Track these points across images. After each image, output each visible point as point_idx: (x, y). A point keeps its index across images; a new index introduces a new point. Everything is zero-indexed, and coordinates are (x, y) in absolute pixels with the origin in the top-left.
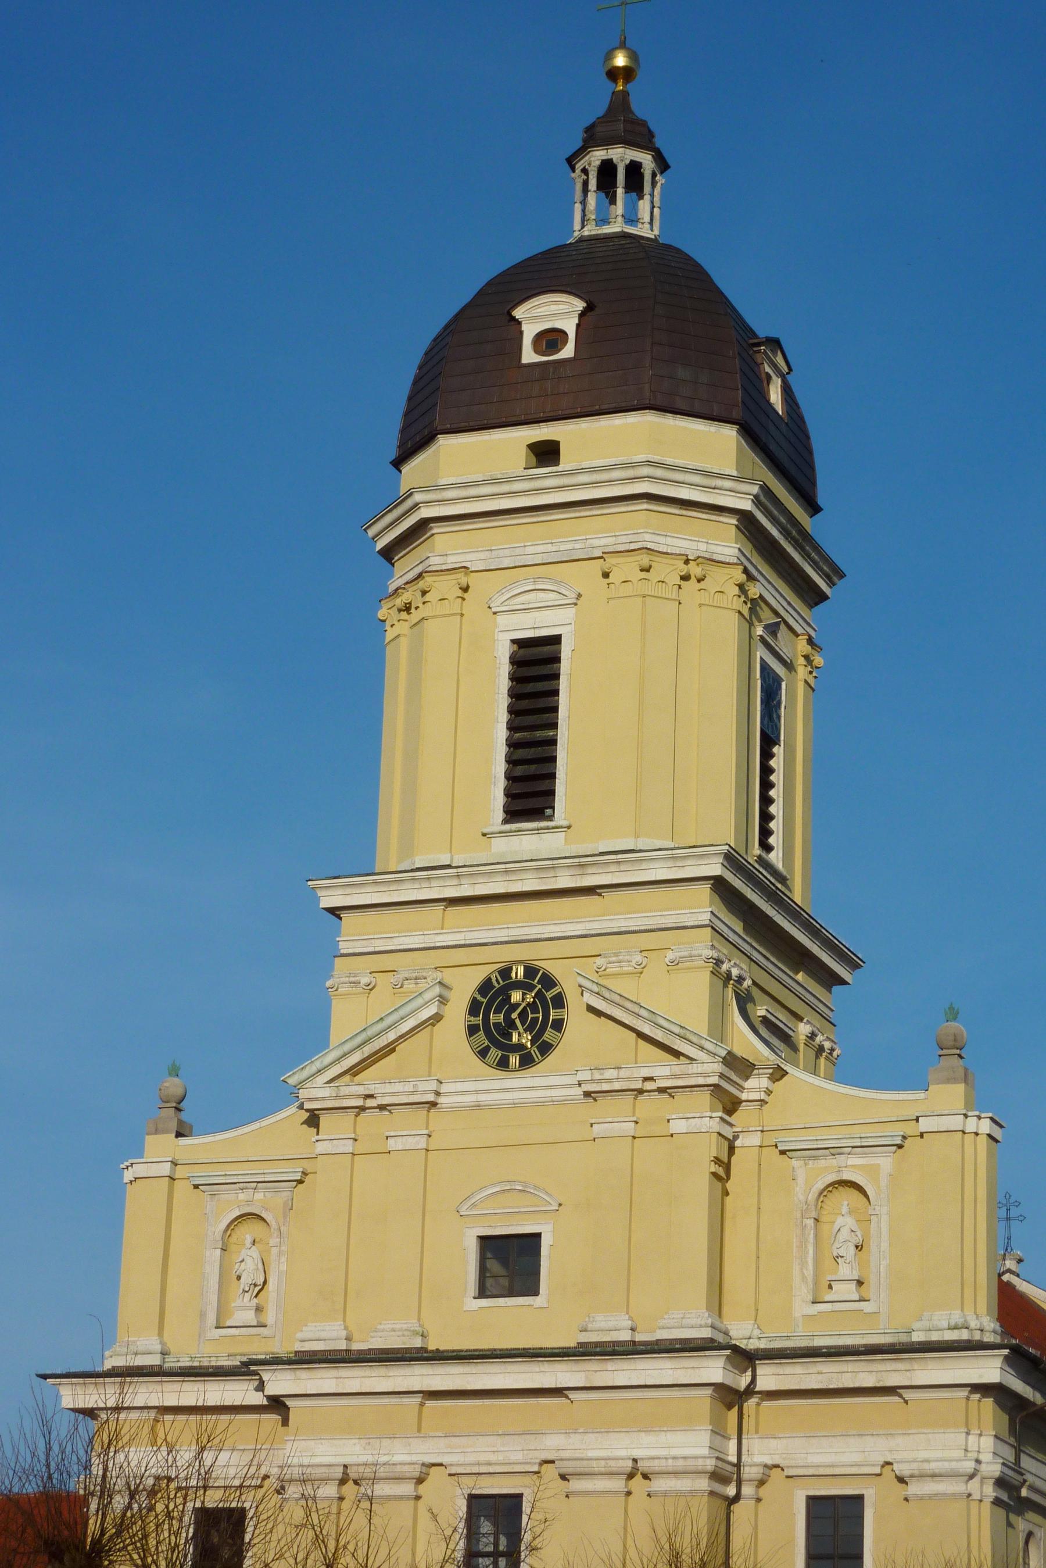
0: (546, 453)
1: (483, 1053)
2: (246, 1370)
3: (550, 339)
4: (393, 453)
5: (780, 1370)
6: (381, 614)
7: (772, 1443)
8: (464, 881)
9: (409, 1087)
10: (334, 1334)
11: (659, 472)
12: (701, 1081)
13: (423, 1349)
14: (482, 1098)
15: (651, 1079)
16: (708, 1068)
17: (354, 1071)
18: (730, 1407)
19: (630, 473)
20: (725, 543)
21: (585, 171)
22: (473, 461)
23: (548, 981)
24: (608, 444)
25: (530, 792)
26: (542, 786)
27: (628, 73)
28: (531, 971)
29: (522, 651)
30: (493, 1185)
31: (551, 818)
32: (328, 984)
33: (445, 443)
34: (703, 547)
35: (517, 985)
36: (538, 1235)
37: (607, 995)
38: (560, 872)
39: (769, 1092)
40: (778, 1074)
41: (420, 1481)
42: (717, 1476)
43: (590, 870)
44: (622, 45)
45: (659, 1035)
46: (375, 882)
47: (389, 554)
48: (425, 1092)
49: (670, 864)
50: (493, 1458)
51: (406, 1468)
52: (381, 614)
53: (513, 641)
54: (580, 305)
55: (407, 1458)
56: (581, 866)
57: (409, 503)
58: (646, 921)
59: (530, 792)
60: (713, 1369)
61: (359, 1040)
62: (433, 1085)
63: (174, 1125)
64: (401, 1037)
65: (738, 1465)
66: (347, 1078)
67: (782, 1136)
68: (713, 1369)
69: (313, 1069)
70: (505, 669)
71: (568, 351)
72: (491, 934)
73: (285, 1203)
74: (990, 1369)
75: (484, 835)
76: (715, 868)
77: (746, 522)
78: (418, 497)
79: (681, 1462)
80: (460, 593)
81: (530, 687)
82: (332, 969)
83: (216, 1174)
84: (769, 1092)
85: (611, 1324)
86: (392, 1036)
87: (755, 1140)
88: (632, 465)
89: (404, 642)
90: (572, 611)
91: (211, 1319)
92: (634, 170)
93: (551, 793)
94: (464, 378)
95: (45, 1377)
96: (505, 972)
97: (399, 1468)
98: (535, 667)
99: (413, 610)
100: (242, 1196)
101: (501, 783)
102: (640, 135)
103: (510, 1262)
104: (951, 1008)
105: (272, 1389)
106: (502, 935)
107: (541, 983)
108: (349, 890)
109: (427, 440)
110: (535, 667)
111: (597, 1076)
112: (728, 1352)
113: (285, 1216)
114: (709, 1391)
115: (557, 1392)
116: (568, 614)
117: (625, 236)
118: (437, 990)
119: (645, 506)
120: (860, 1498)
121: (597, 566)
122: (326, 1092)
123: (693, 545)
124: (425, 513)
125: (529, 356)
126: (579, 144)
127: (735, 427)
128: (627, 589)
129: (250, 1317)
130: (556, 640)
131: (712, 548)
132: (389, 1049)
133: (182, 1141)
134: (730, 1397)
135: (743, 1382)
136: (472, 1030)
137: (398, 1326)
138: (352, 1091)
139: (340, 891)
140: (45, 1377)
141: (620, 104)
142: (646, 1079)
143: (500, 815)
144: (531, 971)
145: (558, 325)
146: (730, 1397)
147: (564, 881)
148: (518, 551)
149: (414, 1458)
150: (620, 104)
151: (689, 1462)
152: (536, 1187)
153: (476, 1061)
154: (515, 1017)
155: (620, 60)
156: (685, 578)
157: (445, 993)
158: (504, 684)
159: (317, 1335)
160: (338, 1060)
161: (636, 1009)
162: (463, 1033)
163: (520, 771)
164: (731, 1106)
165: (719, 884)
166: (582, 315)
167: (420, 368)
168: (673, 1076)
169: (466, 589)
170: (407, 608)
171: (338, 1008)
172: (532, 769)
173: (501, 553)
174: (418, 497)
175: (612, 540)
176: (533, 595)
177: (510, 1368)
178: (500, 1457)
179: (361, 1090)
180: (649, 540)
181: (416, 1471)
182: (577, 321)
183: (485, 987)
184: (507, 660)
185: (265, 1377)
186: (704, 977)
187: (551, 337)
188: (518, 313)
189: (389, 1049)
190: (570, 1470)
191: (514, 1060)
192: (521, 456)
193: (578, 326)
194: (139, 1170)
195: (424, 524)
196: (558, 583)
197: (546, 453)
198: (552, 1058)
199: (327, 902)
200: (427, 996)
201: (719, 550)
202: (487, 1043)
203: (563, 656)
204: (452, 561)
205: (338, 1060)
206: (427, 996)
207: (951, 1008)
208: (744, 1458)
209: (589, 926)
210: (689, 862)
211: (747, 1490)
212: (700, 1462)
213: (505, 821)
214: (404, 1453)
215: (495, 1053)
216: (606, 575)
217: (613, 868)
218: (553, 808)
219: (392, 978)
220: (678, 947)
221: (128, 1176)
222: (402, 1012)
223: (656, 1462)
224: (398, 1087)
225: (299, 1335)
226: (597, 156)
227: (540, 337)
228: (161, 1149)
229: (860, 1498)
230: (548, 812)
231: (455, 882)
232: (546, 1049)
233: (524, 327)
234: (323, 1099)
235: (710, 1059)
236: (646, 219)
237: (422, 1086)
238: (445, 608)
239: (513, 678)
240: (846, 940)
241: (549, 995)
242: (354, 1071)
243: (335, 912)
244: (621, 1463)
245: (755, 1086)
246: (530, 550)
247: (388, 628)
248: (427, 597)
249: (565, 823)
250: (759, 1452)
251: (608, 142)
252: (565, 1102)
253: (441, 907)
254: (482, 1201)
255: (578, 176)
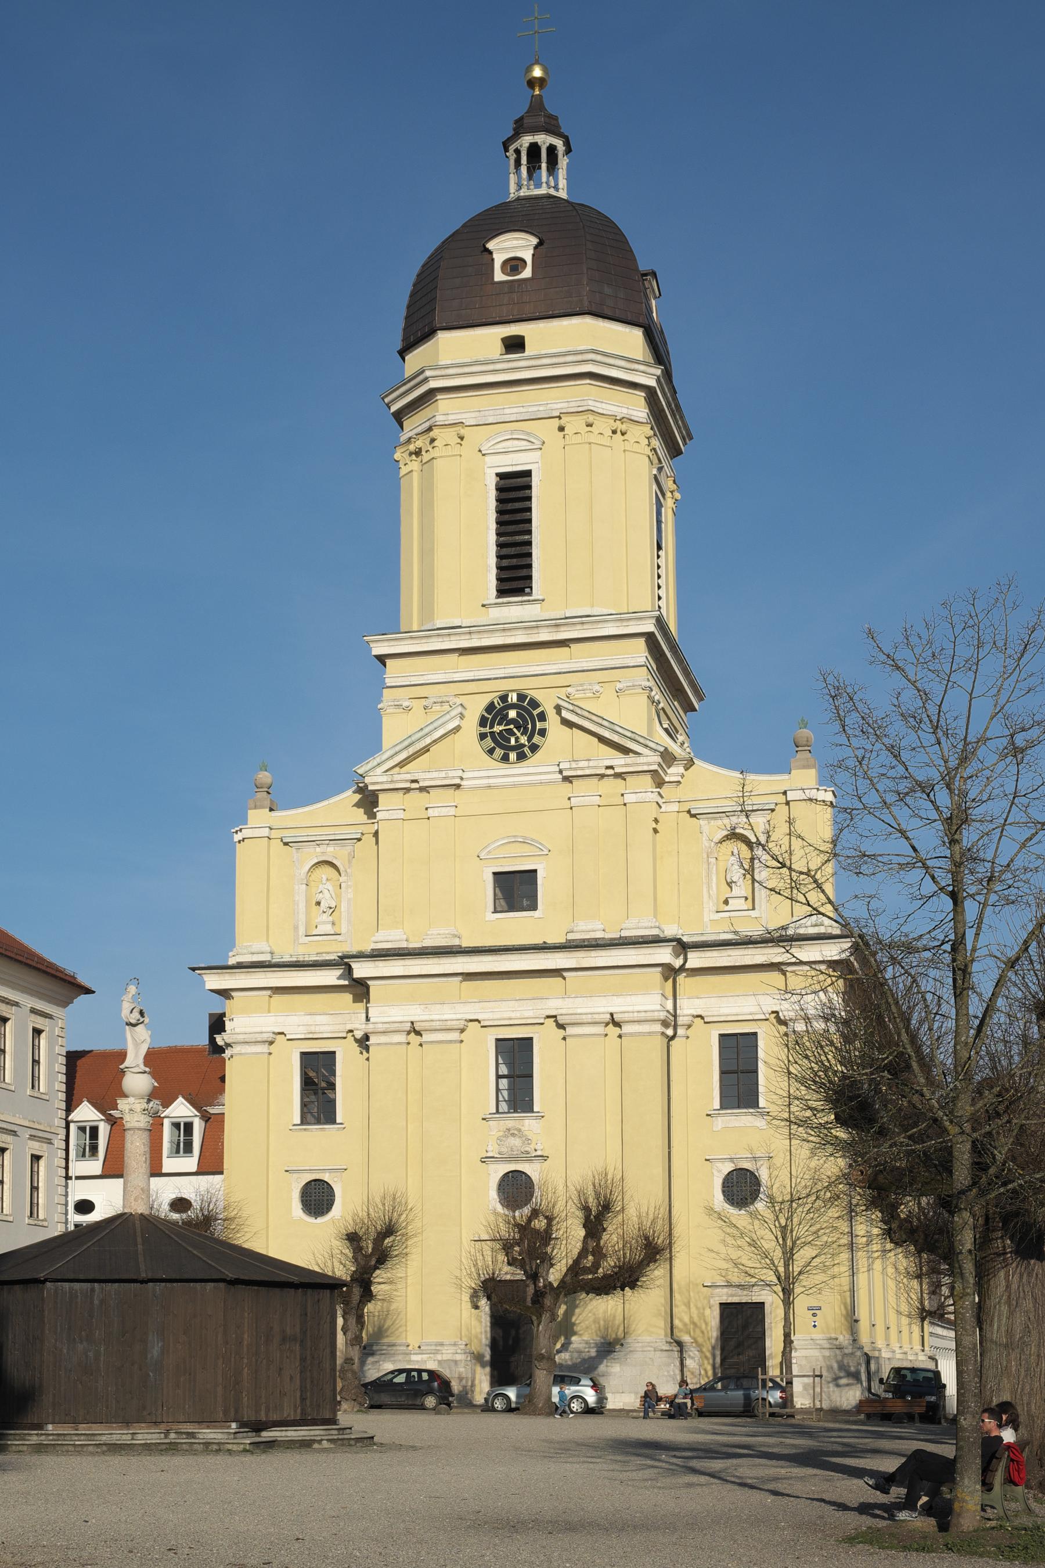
0: (514, 345)
1: (491, 752)
2: (344, 963)
3: (514, 265)
4: (399, 347)
5: (702, 954)
6: (397, 456)
7: (697, 999)
8: (473, 636)
9: (443, 774)
10: (398, 938)
11: (599, 358)
12: (646, 768)
13: (460, 947)
14: (491, 781)
15: (612, 767)
16: (650, 760)
17: (401, 764)
18: (666, 979)
19: (579, 358)
20: (637, 407)
21: (518, 152)
22: (460, 350)
23: (534, 704)
24: (554, 338)
25: (514, 576)
26: (523, 573)
27: (541, 82)
28: (521, 697)
29: (502, 482)
30: (503, 838)
31: (530, 594)
32: (379, 706)
33: (442, 336)
34: (625, 411)
35: (513, 706)
36: (535, 871)
37: (579, 711)
38: (541, 630)
39: (683, 776)
40: (689, 764)
41: (462, 1031)
42: (665, 1024)
43: (562, 629)
44: (537, 62)
45: (615, 738)
46: (411, 638)
47: (399, 417)
48: (454, 777)
49: (618, 624)
50: (513, 1015)
51: (454, 1023)
52: (397, 456)
53: (497, 475)
54: (534, 241)
55: (454, 1017)
56: (557, 625)
57: (421, 377)
58: (601, 663)
59: (514, 576)
60: (664, 955)
61: (406, 743)
62: (460, 773)
63: (268, 803)
64: (434, 741)
65: (675, 1016)
66: (397, 769)
67: (693, 805)
68: (664, 955)
69: (375, 763)
70: (492, 494)
71: (527, 273)
72: (493, 672)
73: (349, 854)
74: (834, 951)
75: (483, 606)
76: (650, 627)
77: (650, 393)
78: (428, 373)
79: (643, 1014)
80: (459, 441)
81: (510, 506)
82: (382, 695)
83: (302, 835)
84: (683, 776)
85: (590, 927)
86: (428, 740)
87: (675, 807)
88: (581, 353)
89: (415, 475)
90: (539, 453)
91: (302, 931)
92: (552, 150)
93: (530, 578)
94: (445, 292)
95: (193, 969)
96: (504, 698)
97: (449, 1023)
98: (514, 494)
99: (423, 453)
100: (318, 849)
101: (494, 571)
102: (553, 129)
103: (516, 889)
104: (803, 720)
105: (357, 974)
106: (501, 673)
107: (528, 706)
108: (392, 643)
109: (428, 334)
110: (514, 494)
111: (574, 765)
112: (674, 943)
113: (350, 862)
114: (659, 969)
115: (557, 972)
116: (535, 456)
117: (549, 197)
118: (460, 709)
119: (588, 381)
120: (755, 1034)
121: (556, 423)
122: (384, 779)
123: (619, 410)
124: (433, 384)
125: (499, 276)
126: (512, 133)
127: (642, 330)
128: (578, 439)
129: (328, 928)
130: (528, 474)
131: (631, 412)
132: (426, 750)
133: (273, 814)
134: (670, 972)
135: (677, 963)
136: (482, 736)
137: (441, 932)
138: (402, 778)
139: (386, 644)
140: (193, 969)
141: (537, 106)
142: (608, 768)
143: (494, 592)
144: (521, 697)
145: (519, 254)
146: (670, 972)
147: (544, 636)
148: (498, 412)
149: (459, 1016)
150: (537, 106)
151: (649, 1014)
152: (532, 840)
153: (486, 757)
154: (512, 727)
155: (537, 72)
156: (614, 432)
157: (464, 712)
158: (492, 504)
159: (386, 939)
160: (392, 757)
161: (600, 721)
162: (475, 738)
163: (505, 563)
164: (660, 783)
165: (649, 637)
166: (536, 248)
167: (414, 285)
168: (626, 765)
169: (462, 438)
170: (418, 453)
171: (387, 723)
172: (514, 562)
173: (487, 413)
174: (428, 373)
175: (565, 405)
176: (510, 442)
177: (524, 956)
178: (518, 1015)
179: (409, 777)
180: (592, 405)
181: (461, 1024)
182: (532, 252)
183: (490, 707)
184: (494, 487)
185: (353, 965)
186: (644, 699)
187: (514, 263)
188: (490, 245)
189: (426, 750)
190: (568, 1021)
191: (513, 756)
192: (498, 347)
193: (533, 255)
194: (246, 833)
195: (432, 393)
196: (528, 434)
197: (514, 345)
198: (539, 754)
199: (378, 649)
200: (453, 713)
201: (635, 413)
202: (493, 745)
203: (534, 484)
204: (452, 419)
205: (392, 757)
206: (453, 713)
207: (803, 720)
208: (678, 1012)
209: (561, 666)
210: (631, 623)
211: (681, 1031)
212: (656, 1014)
213: (498, 597)
214: (453, 1013)
215: (499, 752)
216: (561, 429)
217: (579, 627)
218: (531, 588)
219: (424, 702)
220: (626, 678)
221: (237, 837)
222: (435, 725)
223: (626, 1015)
224: (435, 775)
225: (374, 939)
226: (526, 140)
227: (505, 263)
228: (259, 819)
229: (755, 1034)
230: (527, 590)
231: (468, 637)
232: (534, 748)
233: (495, 256)
234: (382, 783)
235: (652, 753)
236: (558, 185)
237: (451, 774)
238: (449, 451)
239: (499, 500)
240: (700, 682)
241: (535, 713)
242: (401, 764)
243: (382, 659)
244: (602, 1016)
245: (674, 772)
246: (507, 411)
247: (401, 465)
248: (436, 443)
249: (541, 597)
250: (687, 1008)
251: (535, 130)
252: (550, 782)
253: (454, 657)
254: (495, 849)
255: (511, 153)
